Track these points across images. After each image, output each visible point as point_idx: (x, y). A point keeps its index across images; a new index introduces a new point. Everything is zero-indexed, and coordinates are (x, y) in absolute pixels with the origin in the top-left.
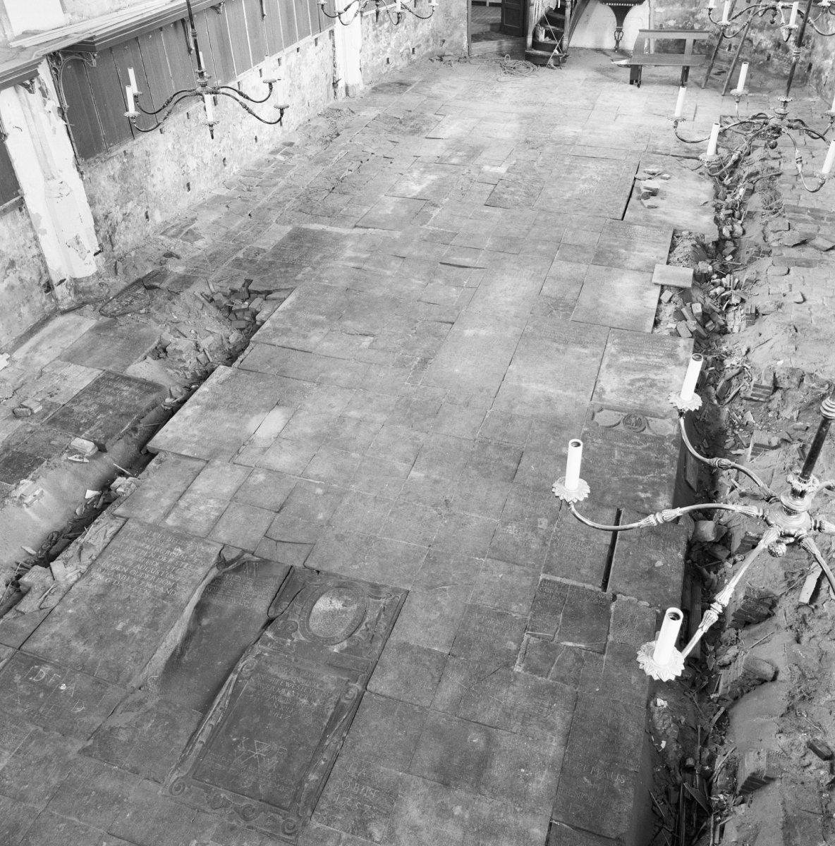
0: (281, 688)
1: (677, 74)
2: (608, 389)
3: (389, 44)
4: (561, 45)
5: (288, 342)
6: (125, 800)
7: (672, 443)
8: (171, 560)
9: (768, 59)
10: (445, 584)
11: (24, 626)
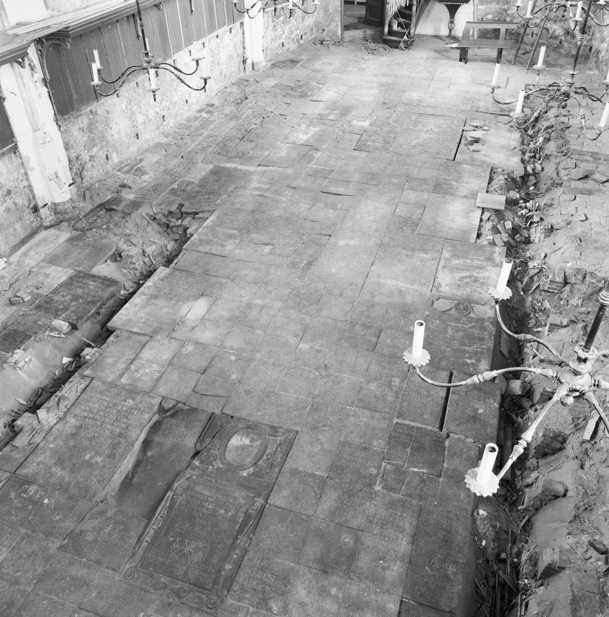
0: (205, 501)
1: (494, 54)
2: (443, 283)
3: (284, 32)
4: (409, 33)
5: (210, 250)
6: (91, 584)
7: (490, 323)
8: (125, 409)
9: (560, 43)
10: (324, 426)
11: (18, 456)
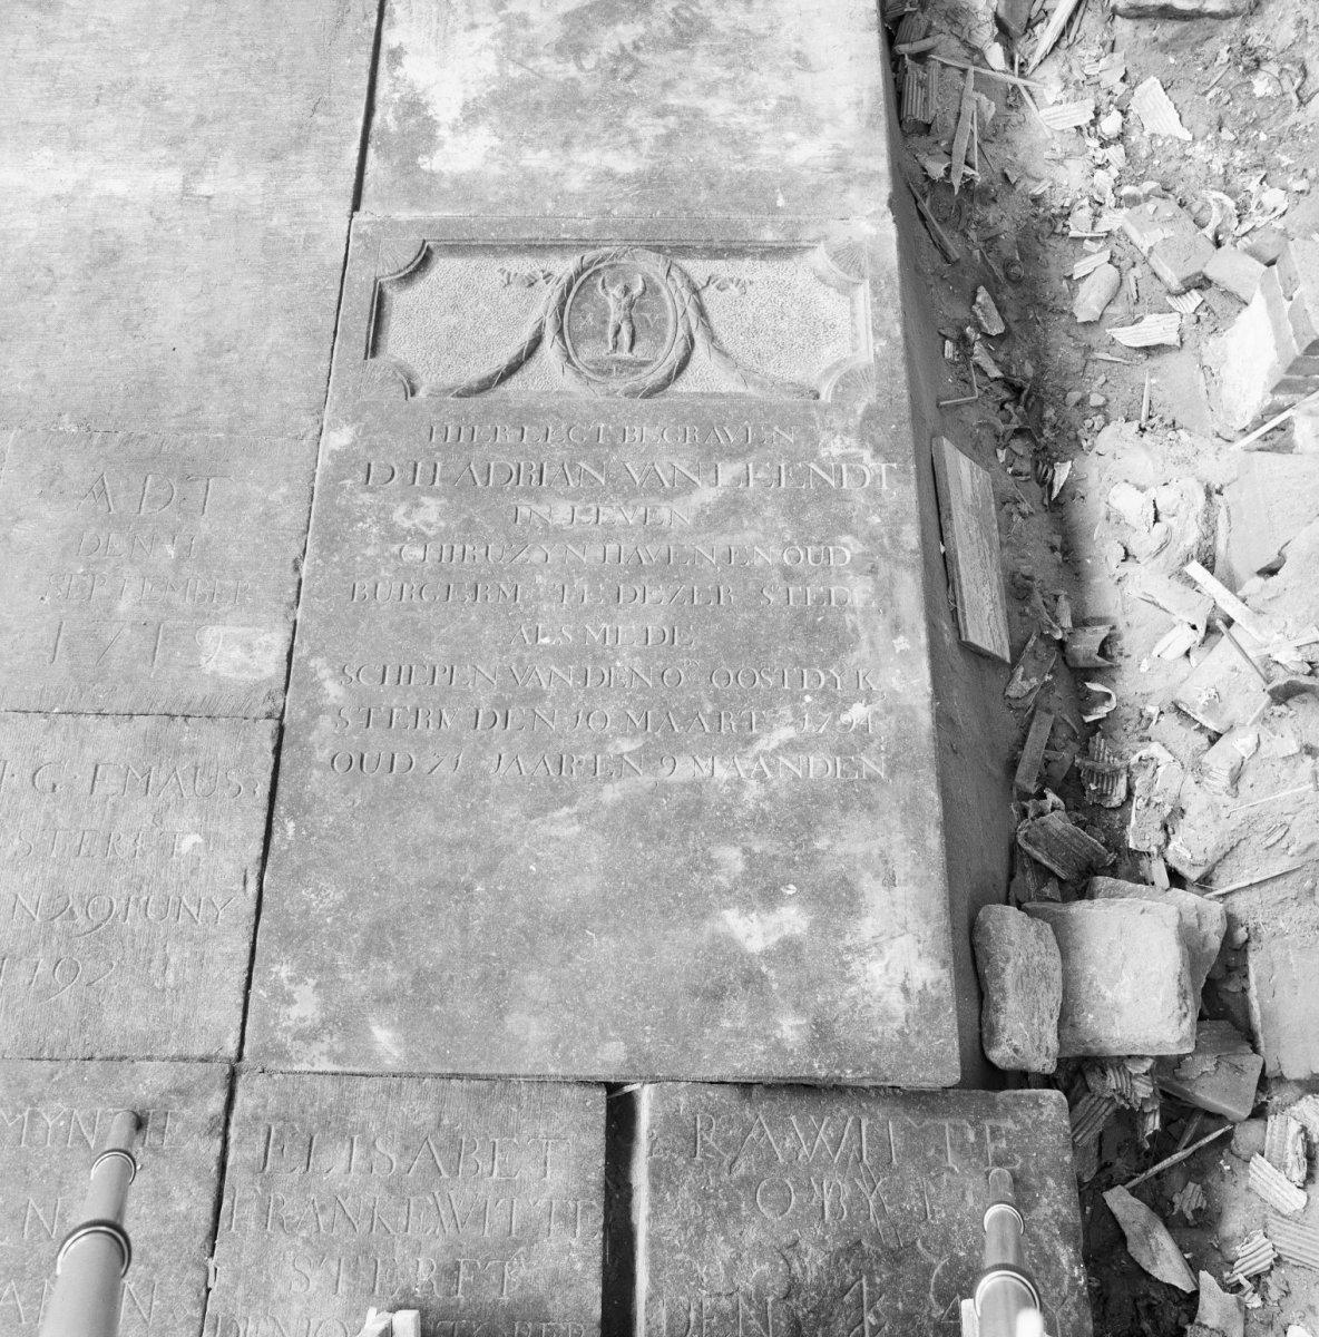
2: (445, 108)
7: (863, 438)
